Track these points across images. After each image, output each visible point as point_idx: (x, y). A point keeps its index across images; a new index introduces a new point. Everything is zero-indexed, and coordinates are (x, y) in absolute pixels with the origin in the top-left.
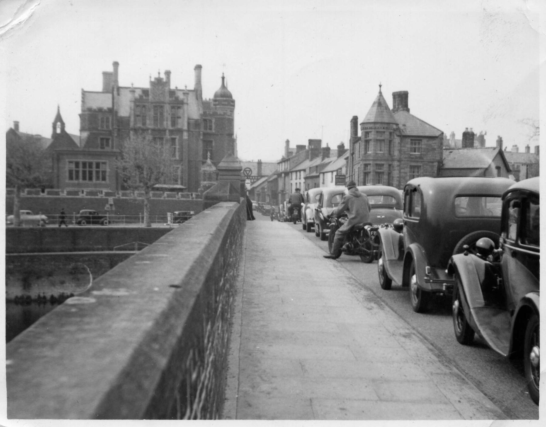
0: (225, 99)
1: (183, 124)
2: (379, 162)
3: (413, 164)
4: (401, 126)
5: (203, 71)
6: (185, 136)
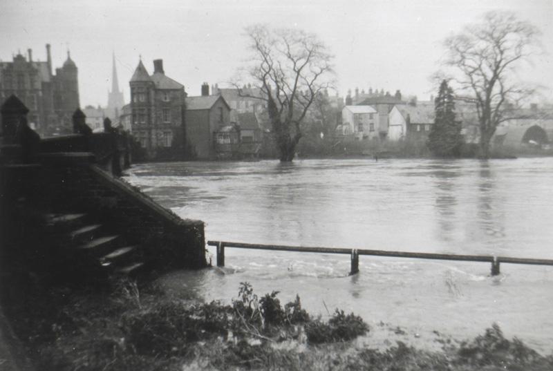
0: (70, 68)
1: (38, 85)
2: (141, 108)
3: (165, 108)
4: (156, 83)
5: (52, 49)
6: (40, 93)
